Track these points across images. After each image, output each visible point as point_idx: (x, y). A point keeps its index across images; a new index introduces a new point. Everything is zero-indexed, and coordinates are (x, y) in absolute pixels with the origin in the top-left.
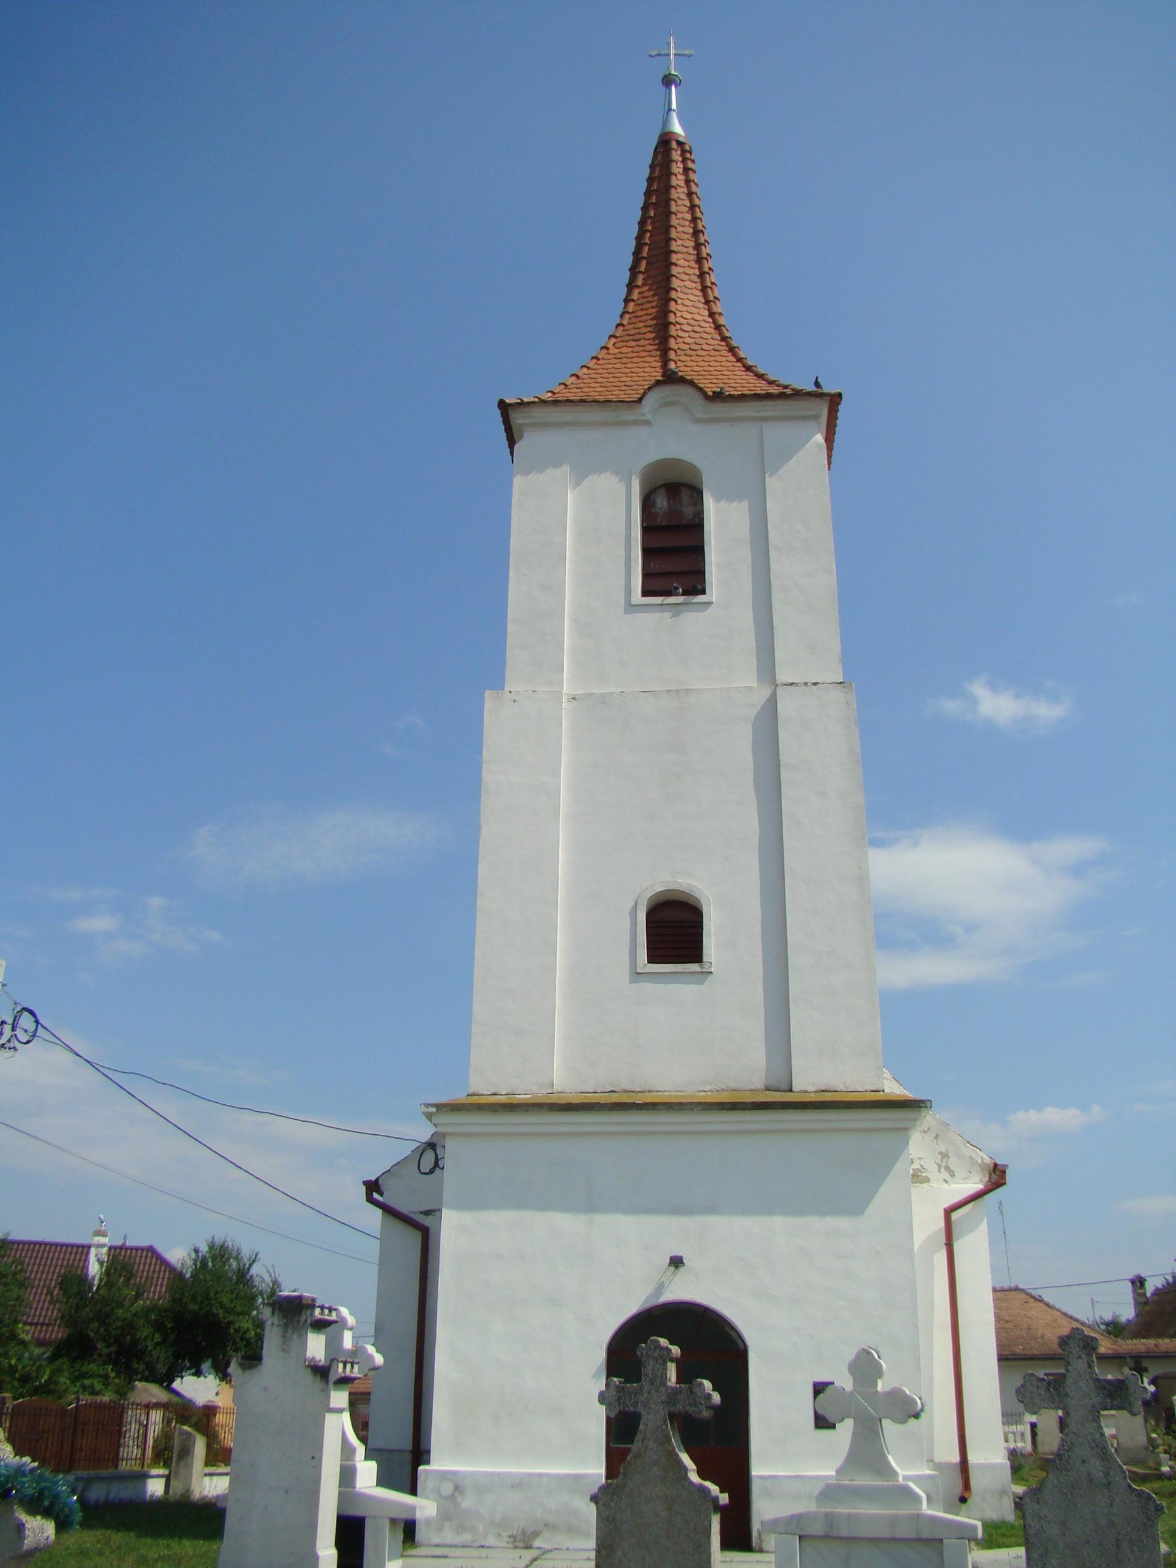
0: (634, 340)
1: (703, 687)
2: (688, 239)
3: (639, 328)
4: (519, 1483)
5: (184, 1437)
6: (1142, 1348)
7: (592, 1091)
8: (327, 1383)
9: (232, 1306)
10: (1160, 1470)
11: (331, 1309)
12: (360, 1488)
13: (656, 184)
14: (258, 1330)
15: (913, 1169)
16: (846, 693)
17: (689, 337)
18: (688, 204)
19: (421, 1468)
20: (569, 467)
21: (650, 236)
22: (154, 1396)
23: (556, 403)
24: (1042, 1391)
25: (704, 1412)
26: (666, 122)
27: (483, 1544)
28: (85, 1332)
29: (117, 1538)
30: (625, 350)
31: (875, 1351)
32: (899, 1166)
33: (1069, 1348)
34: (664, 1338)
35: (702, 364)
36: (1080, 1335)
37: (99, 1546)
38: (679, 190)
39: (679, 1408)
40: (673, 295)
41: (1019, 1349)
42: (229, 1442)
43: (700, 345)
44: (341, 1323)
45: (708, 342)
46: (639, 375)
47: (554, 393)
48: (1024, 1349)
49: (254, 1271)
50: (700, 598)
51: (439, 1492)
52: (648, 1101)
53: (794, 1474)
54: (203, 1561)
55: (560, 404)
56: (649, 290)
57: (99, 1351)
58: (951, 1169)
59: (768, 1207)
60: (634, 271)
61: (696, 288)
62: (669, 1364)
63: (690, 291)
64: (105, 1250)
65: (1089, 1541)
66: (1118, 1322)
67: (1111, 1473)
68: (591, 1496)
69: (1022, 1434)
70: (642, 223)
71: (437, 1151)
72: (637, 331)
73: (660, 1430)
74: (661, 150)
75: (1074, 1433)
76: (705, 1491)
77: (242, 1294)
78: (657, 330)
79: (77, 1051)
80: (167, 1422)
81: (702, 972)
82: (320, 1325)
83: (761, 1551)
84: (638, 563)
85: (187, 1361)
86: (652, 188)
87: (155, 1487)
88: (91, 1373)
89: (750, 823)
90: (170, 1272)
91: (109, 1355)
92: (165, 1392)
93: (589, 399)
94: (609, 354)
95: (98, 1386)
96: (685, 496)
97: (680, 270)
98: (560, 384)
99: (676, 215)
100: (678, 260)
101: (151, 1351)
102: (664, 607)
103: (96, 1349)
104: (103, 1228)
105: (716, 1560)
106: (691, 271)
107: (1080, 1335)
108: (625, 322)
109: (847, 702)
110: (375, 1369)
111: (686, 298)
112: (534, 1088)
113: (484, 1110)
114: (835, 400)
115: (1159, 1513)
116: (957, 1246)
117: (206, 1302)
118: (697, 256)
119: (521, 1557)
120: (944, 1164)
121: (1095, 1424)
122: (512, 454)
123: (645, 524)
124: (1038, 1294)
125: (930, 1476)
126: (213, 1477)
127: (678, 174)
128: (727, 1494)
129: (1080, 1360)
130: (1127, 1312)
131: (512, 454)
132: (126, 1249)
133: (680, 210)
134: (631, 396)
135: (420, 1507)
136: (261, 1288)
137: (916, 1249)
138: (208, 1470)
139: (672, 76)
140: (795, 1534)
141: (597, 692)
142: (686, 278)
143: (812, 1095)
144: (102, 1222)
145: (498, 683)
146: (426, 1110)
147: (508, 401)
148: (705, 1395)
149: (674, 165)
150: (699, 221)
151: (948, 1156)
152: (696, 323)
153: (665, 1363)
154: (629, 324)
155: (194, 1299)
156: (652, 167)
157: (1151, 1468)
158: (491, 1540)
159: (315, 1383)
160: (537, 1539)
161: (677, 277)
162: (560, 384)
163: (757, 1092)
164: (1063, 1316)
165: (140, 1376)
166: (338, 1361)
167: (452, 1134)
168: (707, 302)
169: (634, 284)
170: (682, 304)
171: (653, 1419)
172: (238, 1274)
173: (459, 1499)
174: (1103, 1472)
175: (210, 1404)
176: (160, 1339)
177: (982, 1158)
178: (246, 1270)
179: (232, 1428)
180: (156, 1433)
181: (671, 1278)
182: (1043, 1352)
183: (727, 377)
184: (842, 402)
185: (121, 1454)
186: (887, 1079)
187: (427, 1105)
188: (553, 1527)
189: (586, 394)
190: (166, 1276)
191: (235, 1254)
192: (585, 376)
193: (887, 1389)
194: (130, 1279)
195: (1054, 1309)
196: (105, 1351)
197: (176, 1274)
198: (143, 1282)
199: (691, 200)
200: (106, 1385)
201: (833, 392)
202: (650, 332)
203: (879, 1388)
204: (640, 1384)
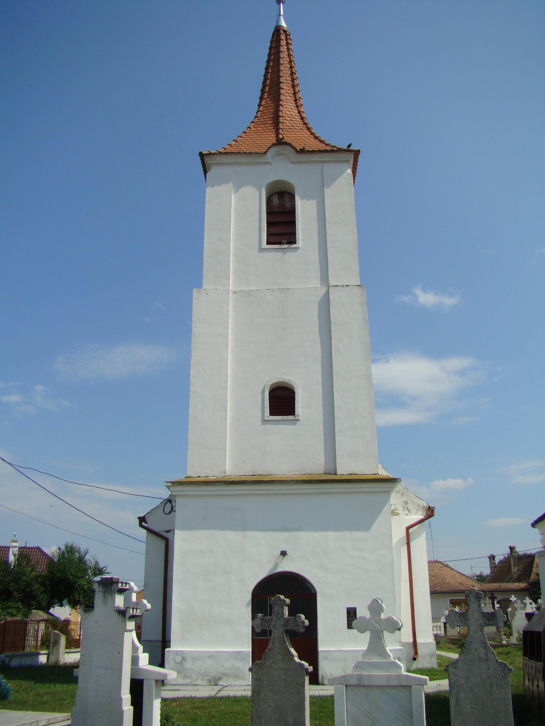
0: (263, 124)
1: (295, 287)
2: (288, 76)
3: (265, 119)
4: (212, 656)
5: (56, 636)
6: (494, 588)
8: (125, 618)
10: (502, 643)
11: (126, 584)
12: (141, 666)
13: (273, 50)
14: (89, 585)
16: (361, 290)
17: (289, 123)
18: (288, 60)
19: (166, 649)
21: (271, 75)
22: (40, 616)
23: (226, 153)
24: (457, 618)
26: (278, 20)
27: (195, 684)
28: (8, 587)
29: (25, 684)
30: (258, 129)
31: (380, 600)
32: (386, 508)
34: (282, 595)
35: (294, 135)
36: (474, 592)
37: (17, 688)
39: (290, 627)
40: (281, 103)
42: (77, 636)
43: (294, 126)
44: (131, 590)
45: (298, 125)
46: (265, 140)
47: (225, 149)
48: (440, 589)
50: (294, 246)
51: (175, 660)
52: (270, 480)
53: (338, 649)
54: (66, 694)
56: (270, 100)
57: (15, 596)
58: (409, 509)
59: (326, 528)
60: (263, 91)
61: (292, 100)
62: (285, 607)
63: (289, 101)
64: (16, 549)
65: (478, 685)
66: (482, 575)
69: (440, 627)
70: (267, 69)
71: (172, 503)
72: (264, 120)
73: (281, 638)
74: (276, 34)
75: (472, 637)
76: (302, 665)
77: (81, 568)
78: (273, 119)
79: (3, 459)
80: (47, 628)
81: (295, 420)
82: (121, 591)
83: (323, 684)
85: (56, 600)
86: (271, 52)
87: (43, 659)
88: (11, 606)
89: (317, 351)
90: (47, 558)
91: (20, 597)
92: (46, 614)
94: (251, 131)
95: (15, 612)
97: (284, 91)
99: (283, 65)
100: (283, 86)
101: (39, 595)
103: (14, 595)
104: (16, 539)
105: (307, 697)
106: (289, 92)
107: (474, 592)
108: (259, 115)
109: (362, 295)
110: (147, 610)
111: (292, 105)
114: (357, 153)
115: (509, 672)
116: (412, 544)
117: (64, 572)
118: (293, 85)
119: (213, 690)
120: (406, 507)
121: (481, 633)
122: (206, 177)
123: (268, 211)
124: (447, 563)
125: (400, 649)
126: (69, 654)
127: (284, 46)
128: (312, 667)
129: (475, 604)
130: (487, 571)
131: (206, 177)
132: (27, 548)
133: (284, 63)
134: (262, 150)
135: (169, 674)
136: (90, 566)
137: (393, 544)
138: (67, 650)
140: (343, 685)
141: (245, 289)
142: (287, 95)
144: (15, 536)
145: (199, 285)
146: (167, 484)
147: (204, 153)
149: (282, 41)
150: (293, 68)
151: (408, 503)
152: (292, 116)
153: (283, 607)
154: (260, 116)
155: (59, 571)
156: (272, 42)
157: (498, 642)
158: (199, 682)
159: (120, 618)
160: (220, 681)
161: (283, 95)
163: (320, 475)
165: (34, 607)
166: (130, 608)
167: (179, 495)
168: (297, 107)
169: (263, 98)
170: (285, 107)
171: (278, 632)
172: (79, 559)
173: (184, 663)
175: (67, 619)
176: (43, 590)
177: (423, 504)
178: (83, 557)
179: (78, 631)
180: (42, 634)
182: (449, 590)
183: (306, 142)
184: (360, 154)
185: (26, 643)
186: (380, 468)
187: (168, 482)
188: (227, 675)
189: (240, 149)
190: (46, 561)
191: (77, 550)
192: (240, 141)
193: (386, 618)
194: (28, 562)
195: (454, 570)
196: (18, 596)
197: (50, 559)
198: (35, 564)
199: (290, 58)
200: (18, 612)
201: (356, 149)
202: (270, 120)
203: (382, 617)
204: (271, 617)
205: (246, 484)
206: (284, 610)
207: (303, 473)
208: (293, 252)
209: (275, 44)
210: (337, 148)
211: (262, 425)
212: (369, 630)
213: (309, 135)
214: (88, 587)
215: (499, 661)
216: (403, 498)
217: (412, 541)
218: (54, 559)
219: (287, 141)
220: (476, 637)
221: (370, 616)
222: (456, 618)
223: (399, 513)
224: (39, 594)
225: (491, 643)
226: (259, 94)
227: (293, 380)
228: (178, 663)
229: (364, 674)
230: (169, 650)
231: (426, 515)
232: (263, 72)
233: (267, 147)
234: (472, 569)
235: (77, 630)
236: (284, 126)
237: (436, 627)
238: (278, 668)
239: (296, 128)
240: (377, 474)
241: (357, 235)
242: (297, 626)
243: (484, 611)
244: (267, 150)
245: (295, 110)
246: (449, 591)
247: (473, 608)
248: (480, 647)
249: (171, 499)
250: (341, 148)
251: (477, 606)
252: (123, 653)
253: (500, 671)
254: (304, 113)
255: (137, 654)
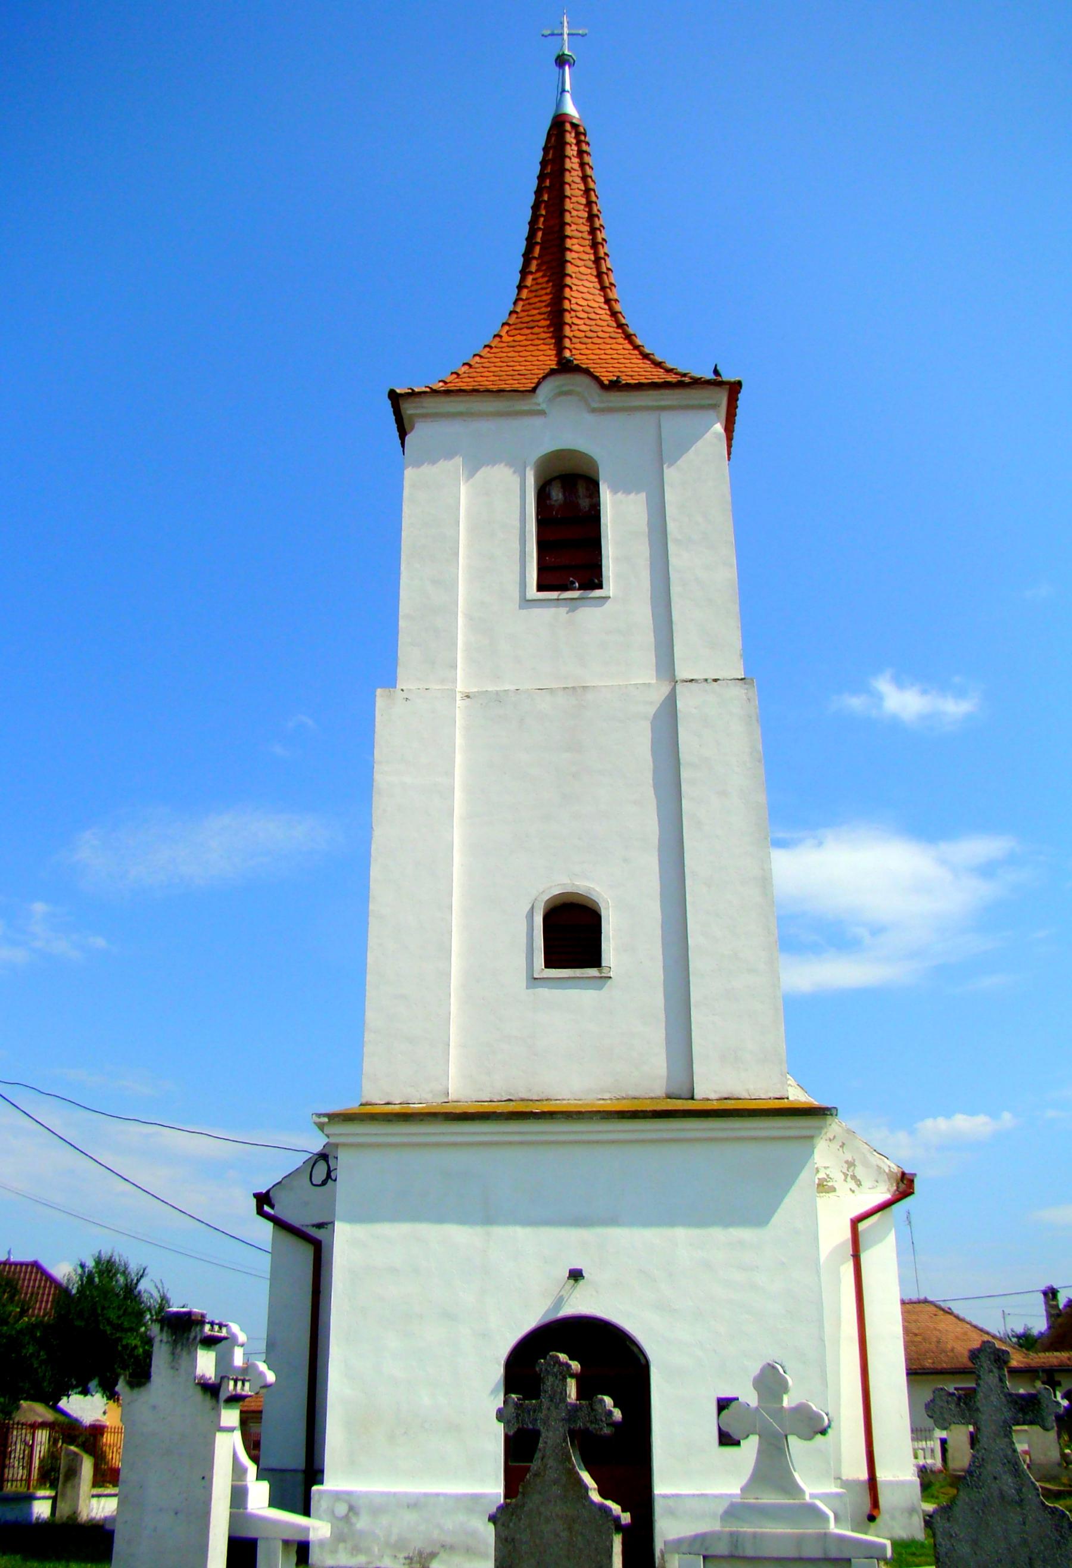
2: (583, 223)
4: (415, 1503)
6: (1055, 1361)
7: (489, 1100)
8: (218, 1401)
9: (120, 1322)
11: (221, 1326)
12: (252, 1509)
13: (549, 167)
15: (819, 1179)
17: (585, 324)
18: (583, 188)
19: (315, 1488)
20: (461, 459)
21: (544, 221)
22: (39, 1415)
23: (447, 392)
24: (953, 1406)
25: (605, 1429)
26: (559, 103)
31: (781, 1365)
32: (805, 1175)
33: (980, 1362)
36: (990, 1348)
38: (574, 173)
39: (580, 1424)
41: (928, 1362)
44: (231, 1339)
45: (604, 329)
47: (445, 383)
48: (933, 1363)
49: (143, 1286)
50: (597, 593)
55: (452, 394)
56: (543, 277)
58: (858, 1178)
60: (527, 256)
61: (591, 274)
62: (569, 1380)
63: (585, 277)
66: (1030, 1335)
67: (1023, 1490)
68: (489, 1516)
69: (932, 1451)
70: (535, 208)
71: (330, 1163)
72: (530, 319)
73: (560, 1448)
74: (555, 132)
75: (985, 1449)
76: (607, 1510)
77: (130, 1310)
78: (551, 317)
80: (52, 1441)
81: (601, 977)
82: (210, 1342)
84: (533, 557)
85: (73, 1380)
87: (42, 1509)
90: (55, 1287)
92: (51, 1411)
93: (482, 388)
96: (581, 490)
98: (452, 373)
99: (570, 199)
100: (573, 245)
102: (560, 602)
106: (586, 257)
107: (990, 1348)
108: (518, 309)
109: (749, 699)
110: (267, 1386)
112: (429, 1097)
113: (377, 1120)
114: (734, 389)
116: (864, 1257)
120: (850, 1173)
121: (1007, 1440)
124: (948, 1306)
125: (837, 1494)
126: (100, 1498)
129: (991, 1374)
130: (1039, 1324)
132: (11, 1264)
134: (526, 385)
135: (313, 1528)
136: (149, 1304)
137: (822, 1261)
138: (96, 1491)
139: (565, 57)
140: (699, 1554)
143: (715, 1103)
147: (398, 391)
148: (606, 1412)
149: (568, 148)
150: (594, 205)
151: (855, 1166)
154: (523, 311)
156: (546, 149)
157: (1064, 1485)
161: (571, 263)
162: (452, 373)
164: (973, 1329)
166: (229, 1379)
167: (344, 1145)
168: (603, 288)
173: (354, 1519)
174: (1016, 1489)
175: (97, 1423)
177: (889, 1167)
179: (120, 1448)
181: (571, 1291)
186: (791, 1086)
187: (319, 1115)
191: (122, 1269)
192: (477, 365)
193: (793, 1405)
197: (61, 1290)
199: (586, 184)
201: (733, 380)
203: (785, 1404)
204: (539, 1400)
205: (492, 1120)
206: (568, 1385)
207: (619, 1095)
208: (596, 606)
209: (553, 154)
210: (691, 378)
211: (527, 988)
212: (756, 1434)
213: (629, 350)
214: (145, 1351)
215: (1050, 1505)
216: (844, 1152)
217: (865, 1251)
218: (70, 1287)
219: (582, 363)
220: (996, 1450)
221: (759, 1402)
222: (950, 1406)
223: (836, 1187)
224: (36, 1366)
225: (1043, 1485)
226: (520, 262)
227: (597, 889)
228: (341, 1519)
229: (745, 1532)
230: (321, 1490)
231: (897, 1193)
232: (528, 214)
233: (537, 378)
234: (1004, 1318)
235: (119, 1445)
236: (574, 332)
237: (923, 1449)
238: (554, 1514)
239: (601, 334)
240: (783, 1099)
241: (737, 569)
242: (595, 1421)
243: (1013, 1392)
244: (538, 384)
245: (598, 296)
246: (953, 1368)
247: (987, 1383)
248: (1005, 1472)
249: (327, 1154)
250: (699, 376)
251: (998, 1379)
252: (212, 1478)
253: (1052, 1528)
254: (618, 301)
255: (244, 1483)
